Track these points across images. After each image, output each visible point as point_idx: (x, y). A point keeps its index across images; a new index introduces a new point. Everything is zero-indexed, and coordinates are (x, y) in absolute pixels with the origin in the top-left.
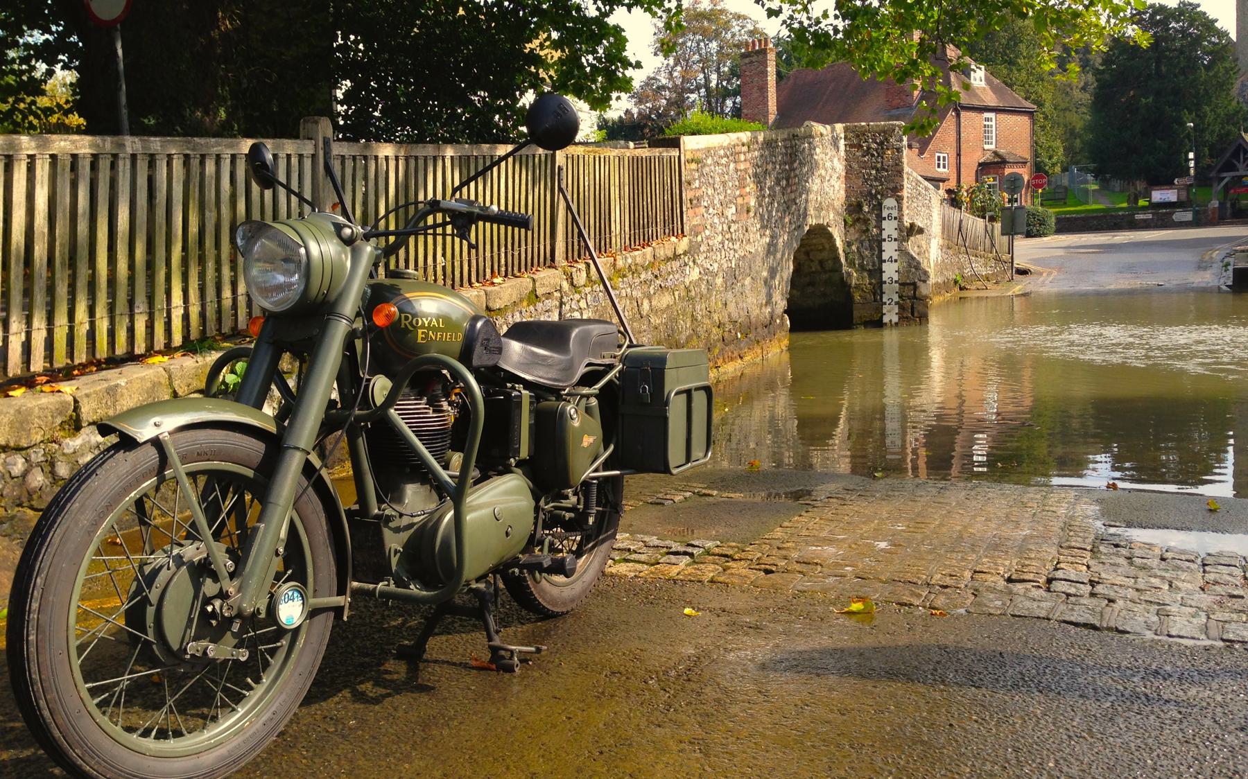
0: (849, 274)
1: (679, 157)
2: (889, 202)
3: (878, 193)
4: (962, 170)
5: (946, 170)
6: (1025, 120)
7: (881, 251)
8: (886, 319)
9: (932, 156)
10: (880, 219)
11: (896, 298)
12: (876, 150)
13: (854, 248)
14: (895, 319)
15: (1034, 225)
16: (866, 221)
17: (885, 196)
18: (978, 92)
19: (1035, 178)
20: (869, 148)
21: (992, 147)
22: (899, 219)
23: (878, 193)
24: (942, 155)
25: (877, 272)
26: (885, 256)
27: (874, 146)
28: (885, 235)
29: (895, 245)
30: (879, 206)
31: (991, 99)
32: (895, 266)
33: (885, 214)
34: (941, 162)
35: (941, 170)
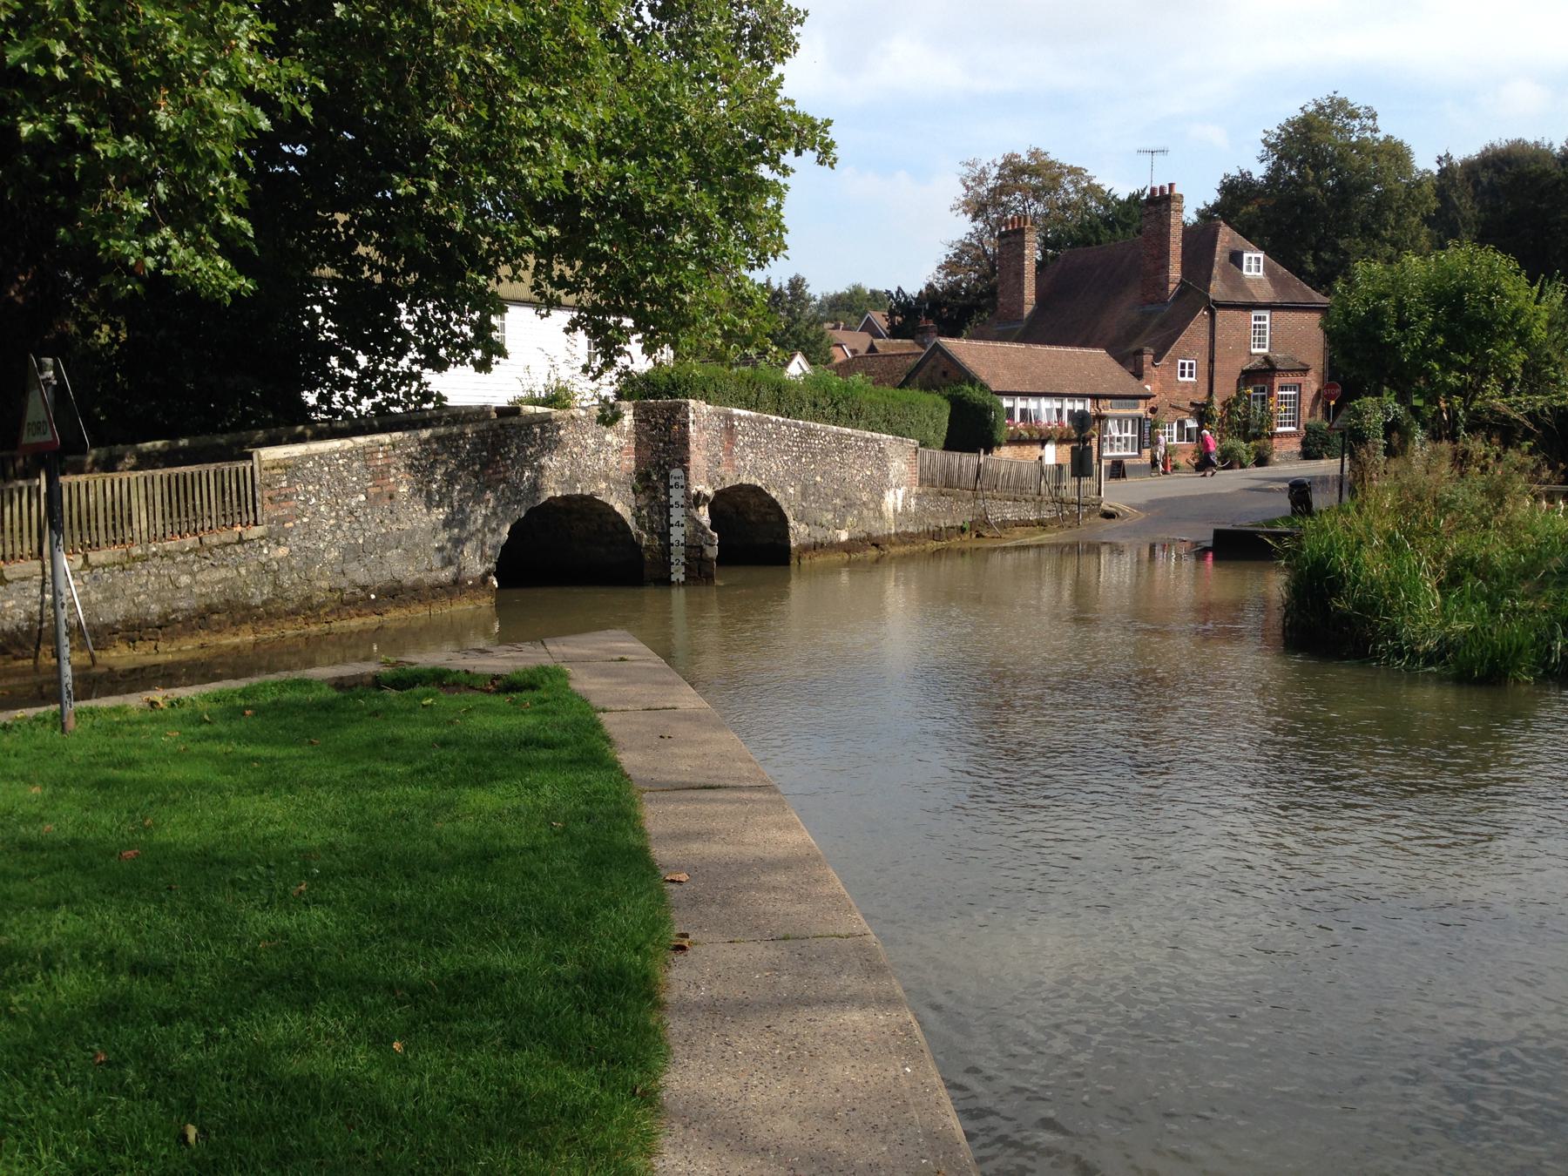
0: (639, 536)
1: (252, 468)
2: (676, 472)
3: (665, 463)
4: (1216, 378)
5: (1193, 379)
6: (1315, 318)
7: (669, 516)
8: (674, 578)
9: (1173, 362)
10: (668, 487)
11: (683, 559)
12: (664, 425)
13: (644, 512)
14: (682, 578)
15: (1315, 445)
16: (655, 489)
17: (672, 467)
18: (1250, 286)
19: (1327, 388)
20: (656, 423)
21: (1265, 351)
22: (687, 487)
23: (665, 463)
24: (1187, 362)
25: (665, 535)
26: (673, 521)
27: (662, 421)
28: (672, 502)
29: (682, 511)
30: (667, 476)
31: (1266, 293)
32: (682, 530)
33: (672, 482)
34: (1187, 370)
35: (1186, 379)
